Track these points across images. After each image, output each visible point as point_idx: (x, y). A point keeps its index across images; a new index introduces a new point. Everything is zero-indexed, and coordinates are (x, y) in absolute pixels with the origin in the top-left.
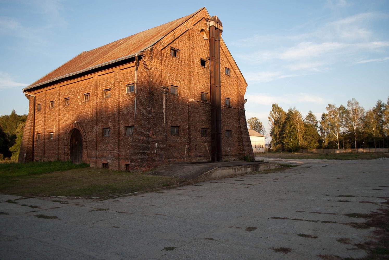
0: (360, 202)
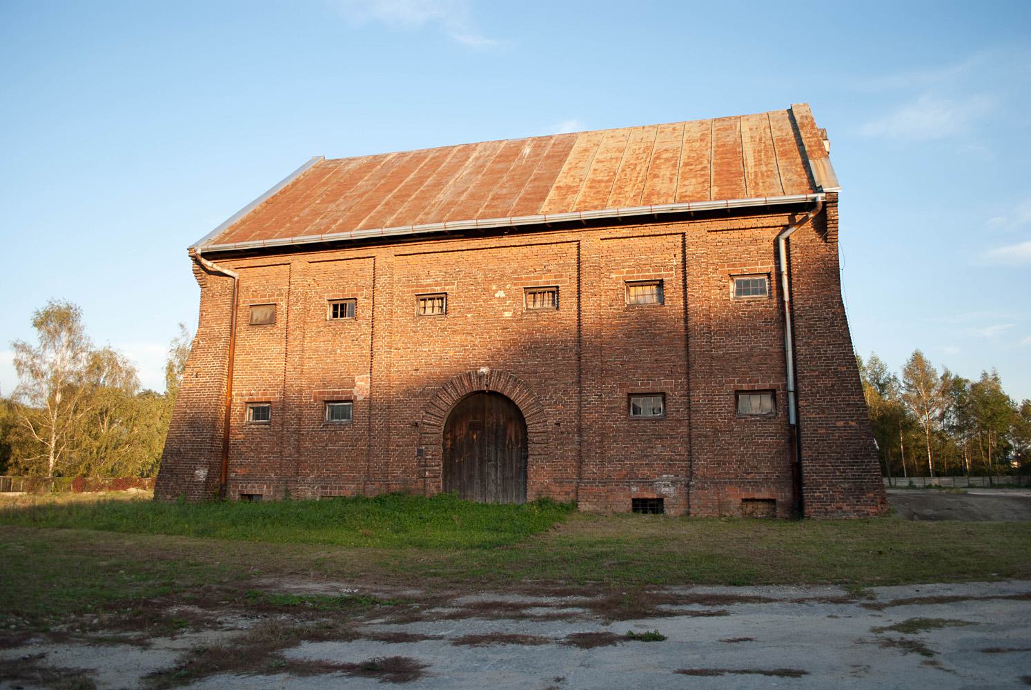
0: (679, 672)
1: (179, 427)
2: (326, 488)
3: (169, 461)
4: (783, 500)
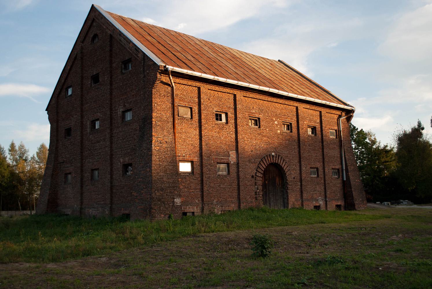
3: (157, 194)
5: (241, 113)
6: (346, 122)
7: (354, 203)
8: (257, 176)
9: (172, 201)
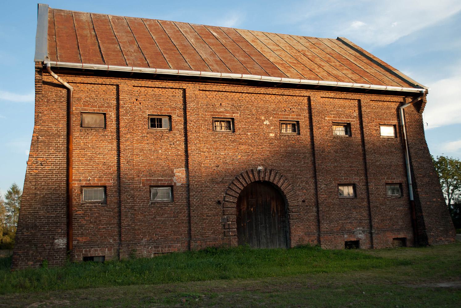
1: (30, 205)
2: (158, 247)
3: (25, 234)
4: (409, 238)
5: (195, 114)
6: (415, 112)
7: (426, 235)
8: (227, 201)
9: (50, 243)
